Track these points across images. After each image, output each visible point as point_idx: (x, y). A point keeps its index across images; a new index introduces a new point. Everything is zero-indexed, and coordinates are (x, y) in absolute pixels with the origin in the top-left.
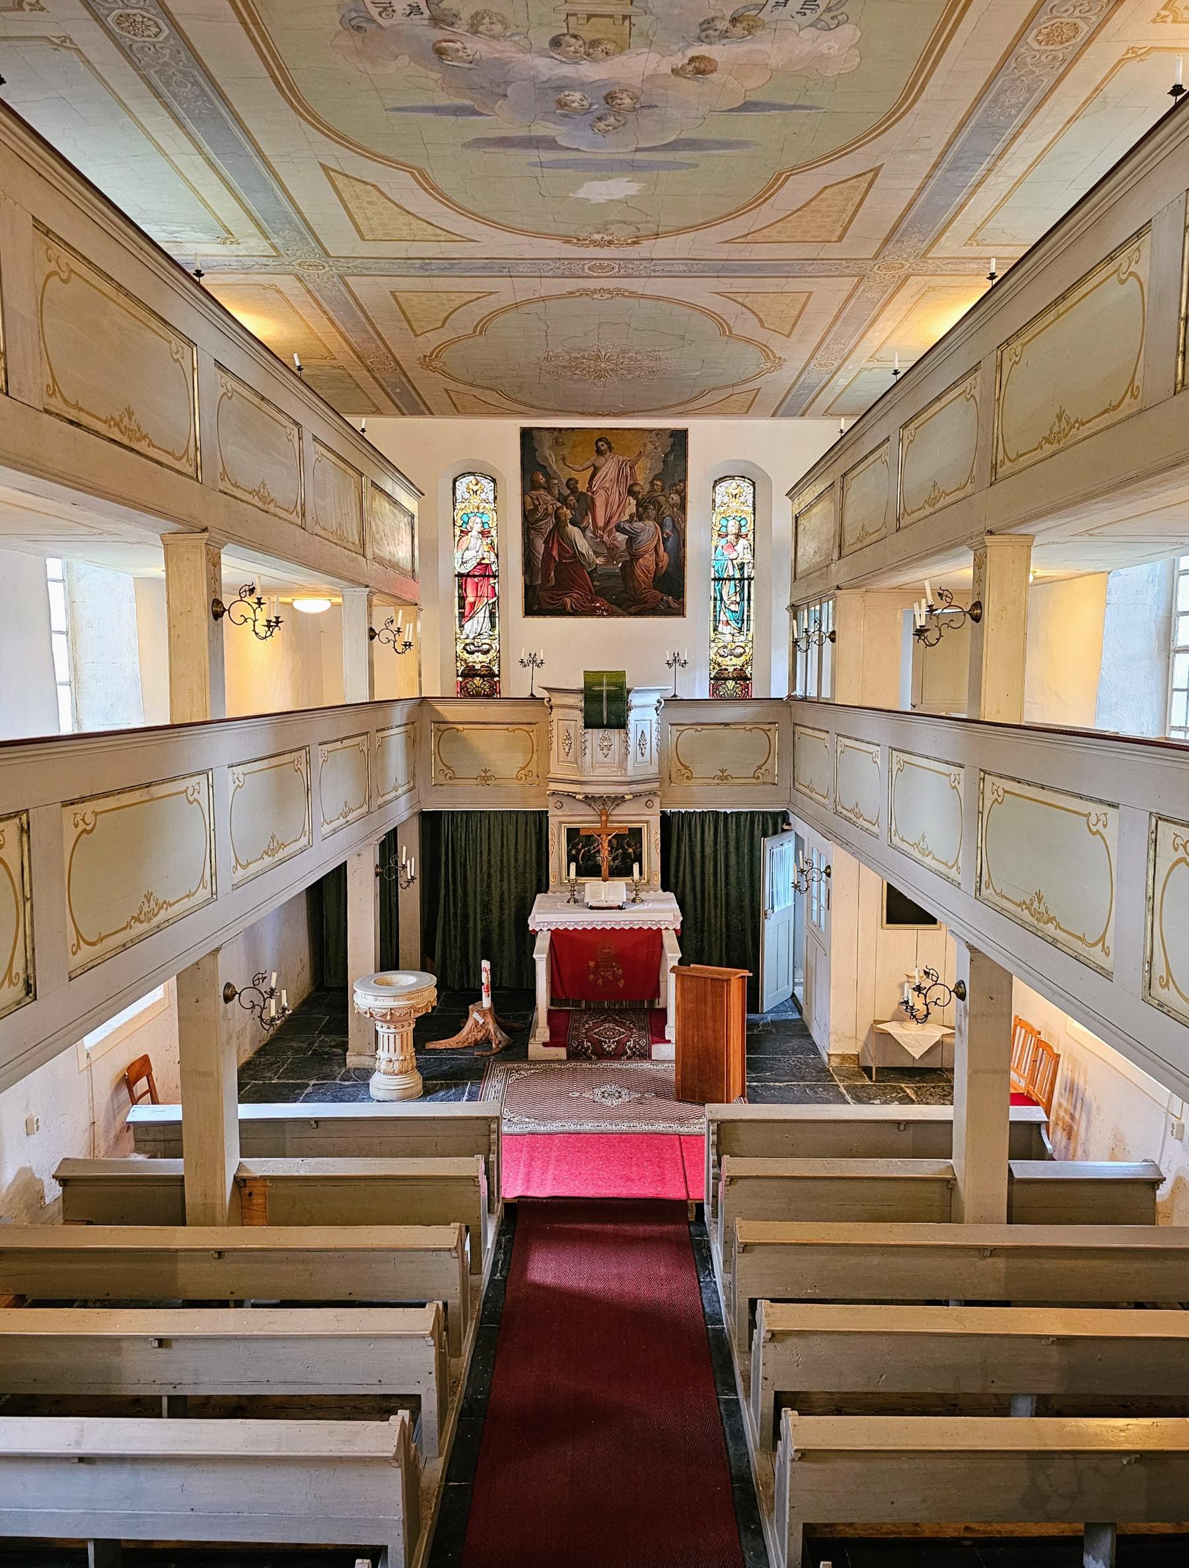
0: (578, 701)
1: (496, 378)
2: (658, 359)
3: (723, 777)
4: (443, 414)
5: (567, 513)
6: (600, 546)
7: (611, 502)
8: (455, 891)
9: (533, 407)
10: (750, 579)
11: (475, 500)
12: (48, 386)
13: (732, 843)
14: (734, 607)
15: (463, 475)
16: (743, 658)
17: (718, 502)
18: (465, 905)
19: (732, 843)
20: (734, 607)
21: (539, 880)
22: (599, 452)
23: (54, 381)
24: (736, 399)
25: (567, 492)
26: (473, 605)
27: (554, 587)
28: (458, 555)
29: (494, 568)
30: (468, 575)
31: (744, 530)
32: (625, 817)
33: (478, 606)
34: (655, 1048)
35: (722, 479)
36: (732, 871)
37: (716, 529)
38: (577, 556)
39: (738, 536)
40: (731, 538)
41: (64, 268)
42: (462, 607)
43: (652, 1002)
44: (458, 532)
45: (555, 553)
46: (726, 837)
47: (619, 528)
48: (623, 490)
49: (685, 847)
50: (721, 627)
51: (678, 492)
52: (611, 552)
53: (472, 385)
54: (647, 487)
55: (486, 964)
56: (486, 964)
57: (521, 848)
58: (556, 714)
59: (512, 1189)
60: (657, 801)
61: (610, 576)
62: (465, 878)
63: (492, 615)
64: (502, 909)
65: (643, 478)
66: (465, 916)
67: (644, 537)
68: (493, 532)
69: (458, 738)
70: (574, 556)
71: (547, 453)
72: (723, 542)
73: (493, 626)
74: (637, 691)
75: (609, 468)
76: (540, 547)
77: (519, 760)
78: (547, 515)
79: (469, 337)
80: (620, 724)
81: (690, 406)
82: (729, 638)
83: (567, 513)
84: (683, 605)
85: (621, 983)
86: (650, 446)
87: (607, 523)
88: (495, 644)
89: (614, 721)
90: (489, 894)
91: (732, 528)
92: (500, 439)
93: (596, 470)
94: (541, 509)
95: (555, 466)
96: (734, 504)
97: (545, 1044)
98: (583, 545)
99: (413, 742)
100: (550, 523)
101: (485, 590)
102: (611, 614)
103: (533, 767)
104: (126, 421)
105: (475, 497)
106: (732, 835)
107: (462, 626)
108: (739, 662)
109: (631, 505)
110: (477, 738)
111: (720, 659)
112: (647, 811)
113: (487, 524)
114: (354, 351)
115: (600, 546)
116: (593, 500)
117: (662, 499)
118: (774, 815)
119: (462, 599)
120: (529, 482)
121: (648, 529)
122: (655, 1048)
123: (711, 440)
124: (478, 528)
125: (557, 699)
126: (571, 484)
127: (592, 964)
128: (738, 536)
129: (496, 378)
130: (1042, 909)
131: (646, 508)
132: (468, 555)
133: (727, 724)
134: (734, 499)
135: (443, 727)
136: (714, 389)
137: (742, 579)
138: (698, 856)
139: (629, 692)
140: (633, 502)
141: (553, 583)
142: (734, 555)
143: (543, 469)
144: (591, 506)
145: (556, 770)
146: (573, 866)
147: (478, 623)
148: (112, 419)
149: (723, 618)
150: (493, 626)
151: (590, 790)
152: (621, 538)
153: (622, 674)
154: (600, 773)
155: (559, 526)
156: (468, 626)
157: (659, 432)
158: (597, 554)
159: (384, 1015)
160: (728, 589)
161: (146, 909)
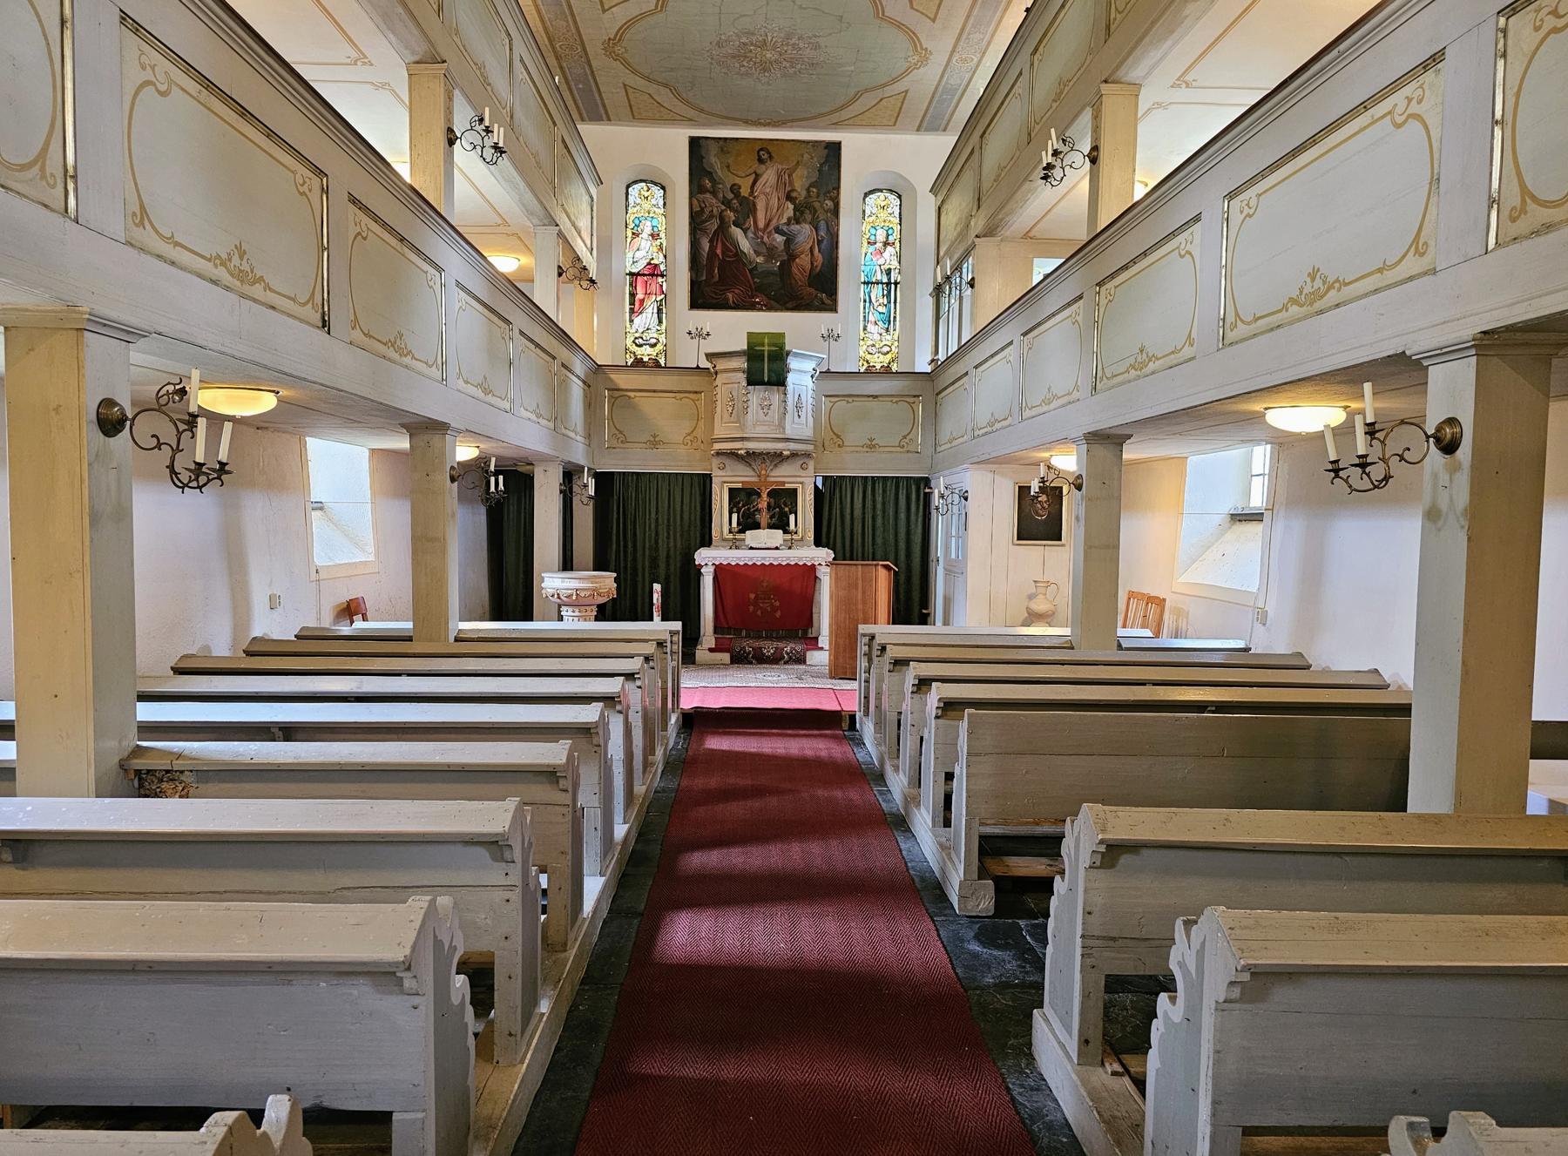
0: (742, 363)
1: (672, 70)
2: (817, 47)
3: (872, 446)
4: (620, 120)
5: (731, 215)
6: (760, 247)
7: (770, 205)
8: (625, 546)
9: (702, 111)
10: (896, 284)
11: (646, 206)
12: (134, 214)
13: (879, 506)
14: (881, 309)
15: (636, 182)
16: (889, 357)
17: (868, 212)
18: (635, 560)
19: (879, 506)
20: (881, 309)
21: (702, 537)
22: (761, 161)
23: (142, 207)
24: (886, 111)
25: (730, 196)
26: (642, 301)
27: (717, 281)
28: (630, 255)
29: (662, 268)
30: (638, 274)
31: (891, 239)
32: (784, 475)
33: (647, 303)
34: (809, 654)
35: (872, 192)
36: (878, 533)
37: (867, 235)
38: (739, 254)
39: (886, 244)
40: (879, 245)
41: (161, 77)
42: (632, 303)
43: (805, 632)
44: (629, 234)
45: (719, 251)
46: (874, 501)
47: (778, 230)
48: (782, 195)
49: (836, 512)
50: (870, 327)
51: (831, 199)
52: (771, 252)
53: (648, 79)
54: (804, 193)
55: (657, 587)
56: (657, 587)
57: (686, 508)
58: (720, 379)
59: (687, 703)
60: (811, 464)
61: (769, 273)
62: (635, 534)
63: (659, 311)
64: (668, 565)
65: (800, 184)
66: (635, 569)
67: (800, 239)
68: (662, 235)
69: (630, 405)
70: (736, 255)
71: (714, 160)
72: (872, 249)
73: (660, 322)
74: (796, 355)
75: (769, 176)
76: (706, 245)
77: (687, 426)
78: (712, 216)
79: (651, 13)
80: (779, 381)
81: (845, 114)
82: (877, 337)
83: (731, 215)
84: (835, 301)
85: (778, 614)
86: (806, 156)
87: (767, 225)
88: (662, 339)
89: (774, 379)
90: (657, 549)
91: (881, 236)
92: (668, 147)
93: (757, 177)
94: (707, 211)
95: (720, 172)
96: (883, 215)
97: (711, 650)
98: (745, 245)
99: (590, 404)
100: (713, 225)
101: (654, 288)
102: (770, 309)
103: (699, 433)
104: (236, 260)
105: (646, 204)
106: (879, 499)
107: (631, 321)
108: (886, 359)
109: (789, 209)
110: (647, 405)
111: (868, 357)
112: (802, 473)
113: (655, 229)
114: (547, 33)
115: (760, 247)
116: (754, 205)
117: (817, 205)
118: (918, 481)
119: (633, 295)
120: (696, 187)
121: (804, 233)
122: (809, 654)
123: (864, 153)
124: (648, 230)
125: (722, 364)
126: (735, 189)
127: (752, 596)
128: (886, 244)
129: (672, 70)
130: (245, 267)
131: (802, 213)
132: (639, 255)
133: (875, 397)
134: (883, 209)
135: (617, 394)
136: (866, 91)
137: (888, 284)
138: (848, 517)
139: (788, 354)
140: (791, 207)
141: (717, 278)
142: (881, 261)
143: (710, 175)
144: (753, 210)
145: (720, 430)
146: (735, 516)
147: (647, 318)
148: (218, 257)
149: (871, 318)
150: (660, 322)
151: (752, 446)
152: (780, 239)
153: (782, 335)
154: (759, 431)
155: (723, 228)
156: (637, 320)
157: (815, 143)
158: (757, 253)
159: (569, 596)
160: (877, 292)
161: (1308, 289)
